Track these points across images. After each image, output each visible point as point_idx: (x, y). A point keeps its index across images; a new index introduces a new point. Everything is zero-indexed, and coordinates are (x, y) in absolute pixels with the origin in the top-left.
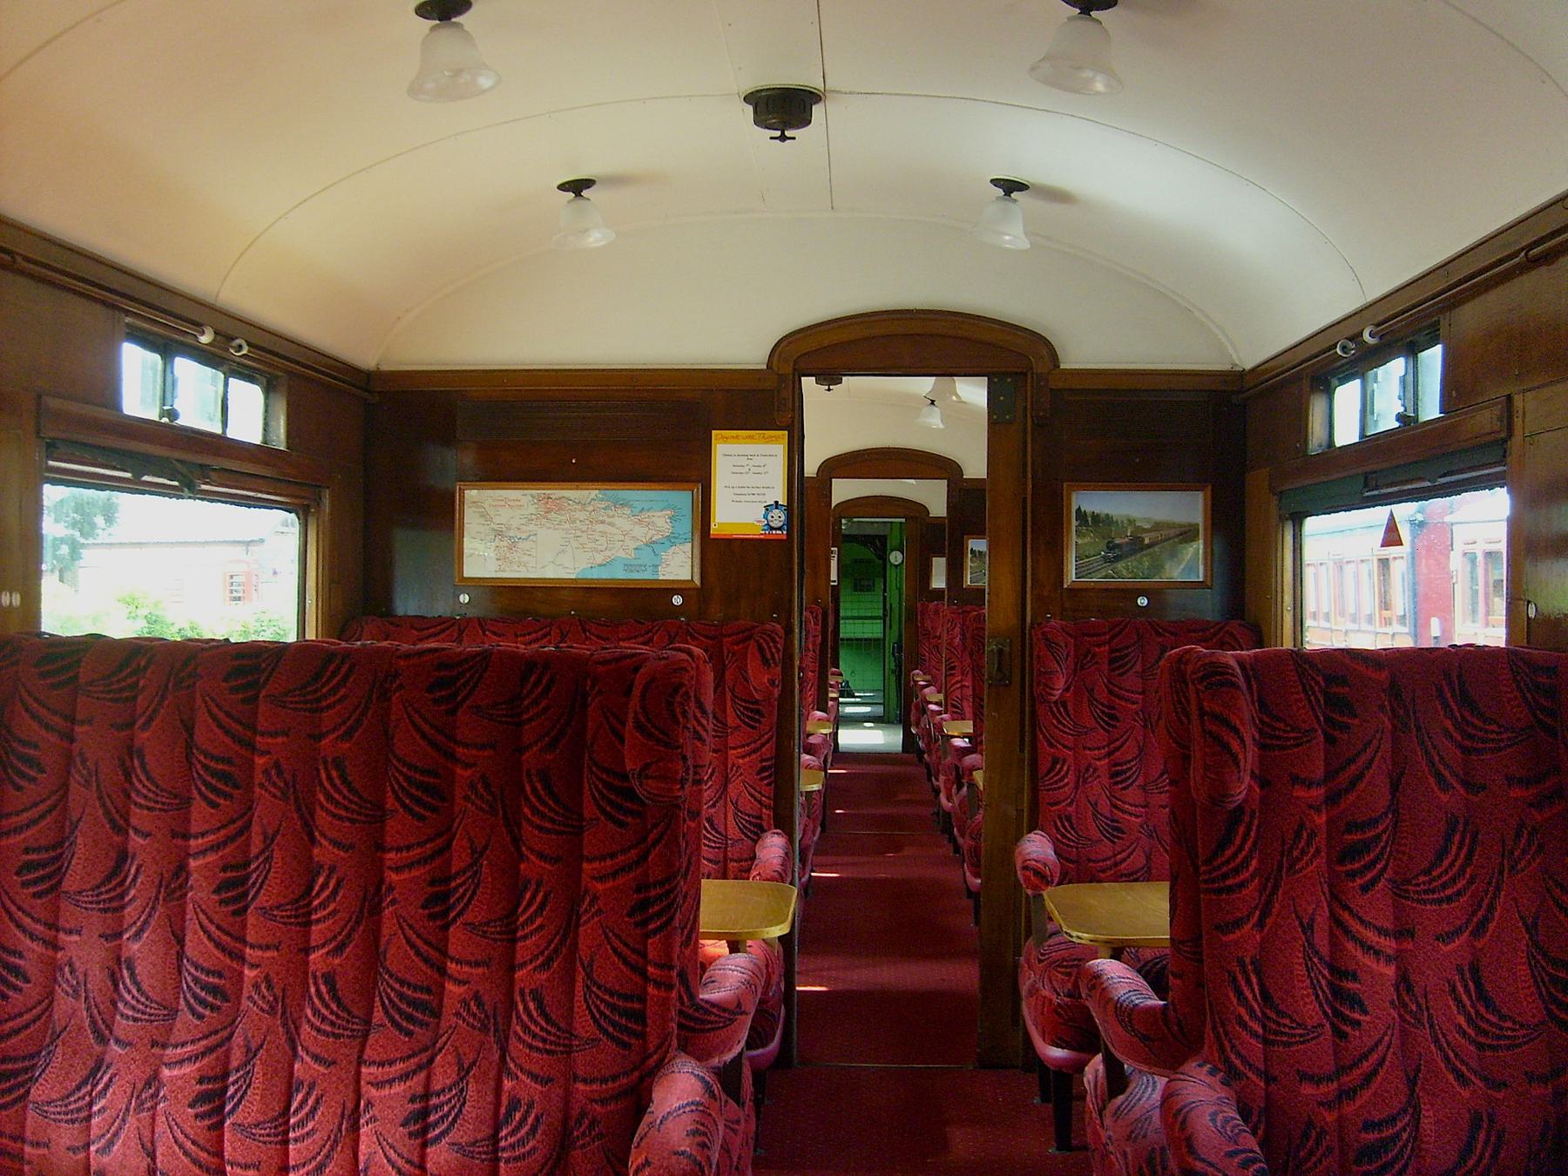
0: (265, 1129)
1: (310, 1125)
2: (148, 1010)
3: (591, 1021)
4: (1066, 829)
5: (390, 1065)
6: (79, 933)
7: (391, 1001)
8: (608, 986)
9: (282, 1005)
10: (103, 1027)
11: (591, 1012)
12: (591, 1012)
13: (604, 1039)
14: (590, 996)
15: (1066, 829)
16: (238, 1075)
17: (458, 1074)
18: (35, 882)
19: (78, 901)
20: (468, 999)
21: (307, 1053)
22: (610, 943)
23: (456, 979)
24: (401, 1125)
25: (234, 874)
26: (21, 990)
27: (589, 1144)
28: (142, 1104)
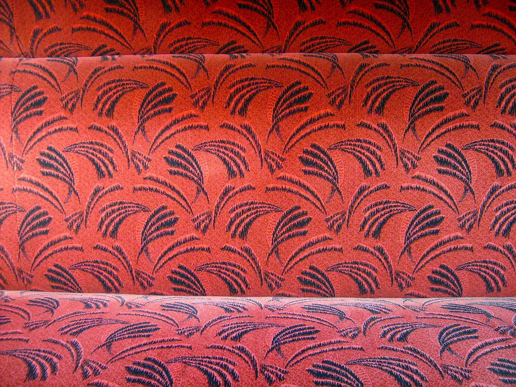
0: (399, 85)
1: (504, 90)
2: (86, 150)
3: (68, 161)
4: (494, 279)
5: (321, 127)
6: (268, 189)
7: (192, 165)
8: (323, 179)
9: (261, 157)
10: (384, 135)
11: (333, 165)
12: (333, 165)
13: (61, 152)
14: (198, 174)
15: (494, 279)
16: (19, 118)
17: (17, 129)
18: (432, 215)
19: (403, 206)
20: (277, 169)
21: (508, 129)
22: (454, 203)
23: (285, 180)
24: (176, 95)
25: (167, 230)
26: (304, 152)
27: (470, 91)
28: (76, 95)
